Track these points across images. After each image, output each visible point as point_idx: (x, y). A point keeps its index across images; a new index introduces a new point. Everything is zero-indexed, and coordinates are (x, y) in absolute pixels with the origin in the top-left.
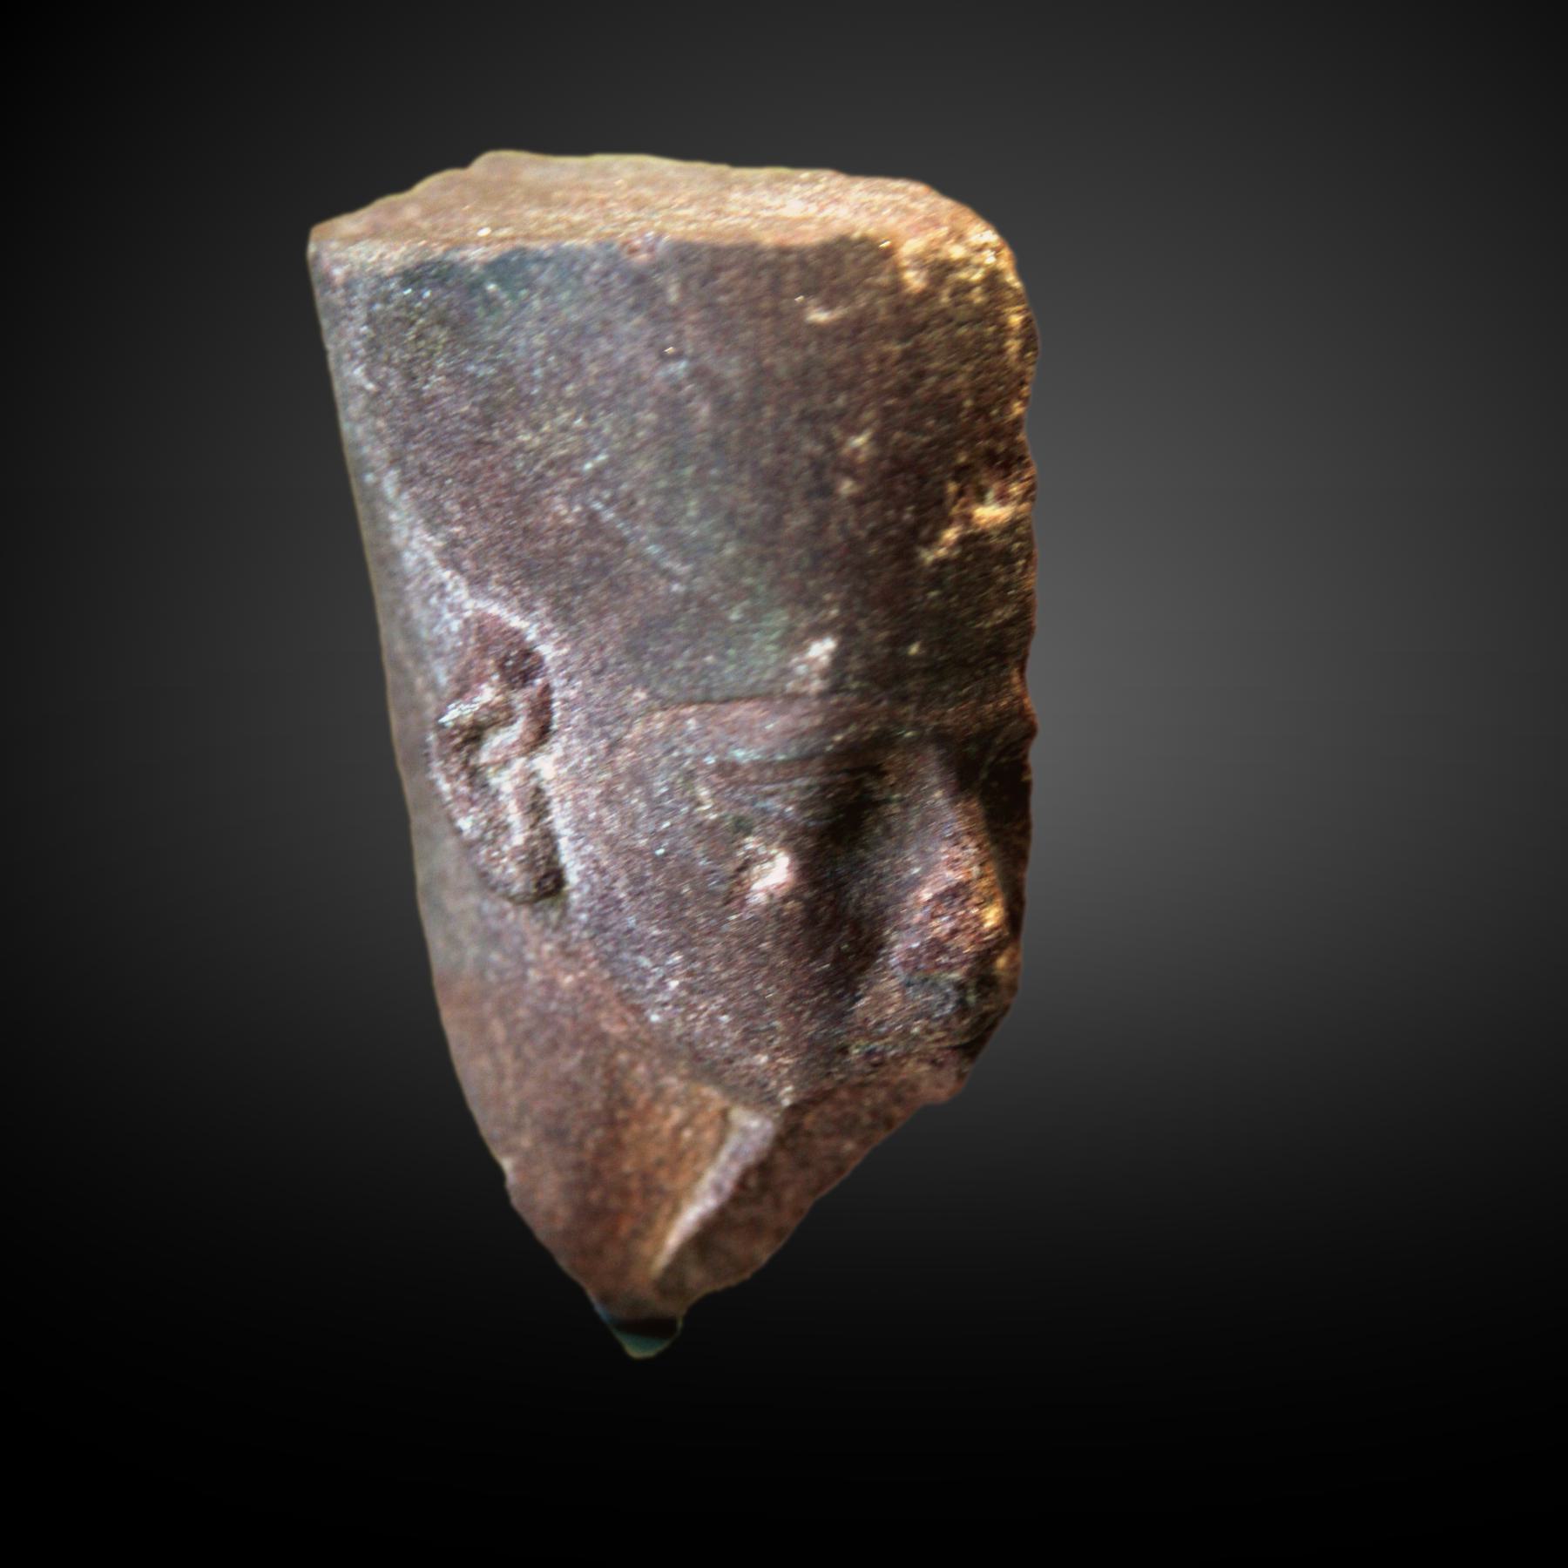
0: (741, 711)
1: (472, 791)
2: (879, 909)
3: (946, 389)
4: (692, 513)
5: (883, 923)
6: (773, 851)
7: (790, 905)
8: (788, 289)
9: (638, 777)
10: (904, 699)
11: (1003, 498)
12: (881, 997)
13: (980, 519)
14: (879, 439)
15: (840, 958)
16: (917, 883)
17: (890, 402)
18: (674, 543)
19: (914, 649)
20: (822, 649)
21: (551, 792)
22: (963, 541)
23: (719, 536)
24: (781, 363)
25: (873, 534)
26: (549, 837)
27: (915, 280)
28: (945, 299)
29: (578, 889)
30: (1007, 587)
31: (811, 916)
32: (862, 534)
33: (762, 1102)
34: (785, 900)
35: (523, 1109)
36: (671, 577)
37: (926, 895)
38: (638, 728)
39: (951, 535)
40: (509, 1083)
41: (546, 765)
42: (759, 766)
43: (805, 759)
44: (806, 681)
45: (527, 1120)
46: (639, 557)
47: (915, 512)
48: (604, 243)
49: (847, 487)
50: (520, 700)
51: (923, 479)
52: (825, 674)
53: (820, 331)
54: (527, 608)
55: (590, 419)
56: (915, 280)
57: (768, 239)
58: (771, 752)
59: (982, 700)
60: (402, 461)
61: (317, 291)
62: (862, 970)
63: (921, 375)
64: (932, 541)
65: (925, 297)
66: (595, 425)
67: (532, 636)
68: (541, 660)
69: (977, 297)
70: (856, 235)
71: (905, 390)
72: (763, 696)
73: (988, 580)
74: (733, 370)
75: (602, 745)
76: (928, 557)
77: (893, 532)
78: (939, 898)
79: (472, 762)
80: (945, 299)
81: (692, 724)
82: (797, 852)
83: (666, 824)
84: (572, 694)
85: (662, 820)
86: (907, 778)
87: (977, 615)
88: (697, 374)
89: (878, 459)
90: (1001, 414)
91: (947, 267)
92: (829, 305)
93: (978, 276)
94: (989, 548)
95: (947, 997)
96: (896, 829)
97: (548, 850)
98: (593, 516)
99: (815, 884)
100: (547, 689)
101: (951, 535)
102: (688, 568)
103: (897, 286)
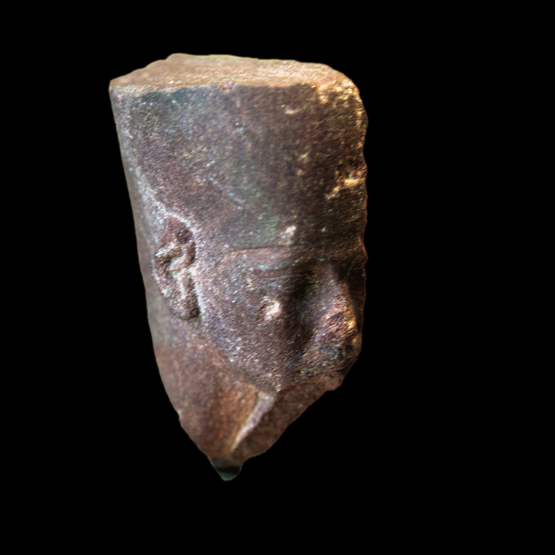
0: (262, 252)
1: (167, 280)
2: (311, 322)
3: (335, 138)
4: (245, 182)
5: (313, 327)
6: (274, 301)
7: (280, 320)
8: (279, 102)
9: (226, 275)
10: (320, 247)
11: (355, 176)
12: (312, 353)
13: (347, 184)
14: (311, 155)
15: (297, 339)
16: (325, 312)
17: (315, 142)
18: (239, 192)
19: (323, 230)
20: (291, 230)
21: (195, 280)
22: (341, 192)
23: (254, 190)
24: (277, 128)
25: (309, 189)
26: (194, 296)
27: (324, 99)
28: (334, 106)
29: (205, 315)
30: (356, 208)
31: (287, 324)
32: (305, 189)
33: (270, 390)
34: (278, 318)
35: (185, 393)
36: (237, 204)
37: (328, 317)
38: (226, 258)
39: (337, 189)
40: (180, 383)
41: (193, 271)
42: (269, 271)
43: (285, 269)
44: (285, 241)
45: (187, 397)
46: (226, 197)
47: (324, 181)
48: (214, 86)
49: (300, 172)
50: (184, 248)
51: (327, 169)
52: (292, 239)
53: (290, 117)
54: (186, 215)
55: (209, 148)
56: (324, 99)
57: (272, 85)
58: (273, 266)
59: (348, 248)
60: (142, 163)
61: (112, 103)
62: (305, 343)
63: (326, 133)
64: (330, 191)
65: (327, 105)
66: (211, 150)
67: (188, 225)
68: (191, 234)
69: (346, 105)
70: (303, 83)
71: (320, 138)
72: (270, 246)
73: (350, 205)
74: (259, 131)
75: (213, 264)
76: (329, 197)
77: (316, 188)
78: (332, 318)
79: (167, 270)
80: (334, 106)
81: (245, 256)
82: (282, 302)
83: (236, 292)
84: (202, 246)
85: (234, 290)
86: (321, 275)
87: (346, 218)
88: (247, 132)
89: (311, 163)
90: (354, 146)
91: (335, 95)
92: (293, 108)
93: (346, 98)
94: (350, 194)
95: (335, 353)
96: (317, 293)
97: (194, 301)
98: (210, 183)
99: (289, 313)
100: (194, 244)
101: (337, 189)
102: (243, 201)
103: (318, 101)
